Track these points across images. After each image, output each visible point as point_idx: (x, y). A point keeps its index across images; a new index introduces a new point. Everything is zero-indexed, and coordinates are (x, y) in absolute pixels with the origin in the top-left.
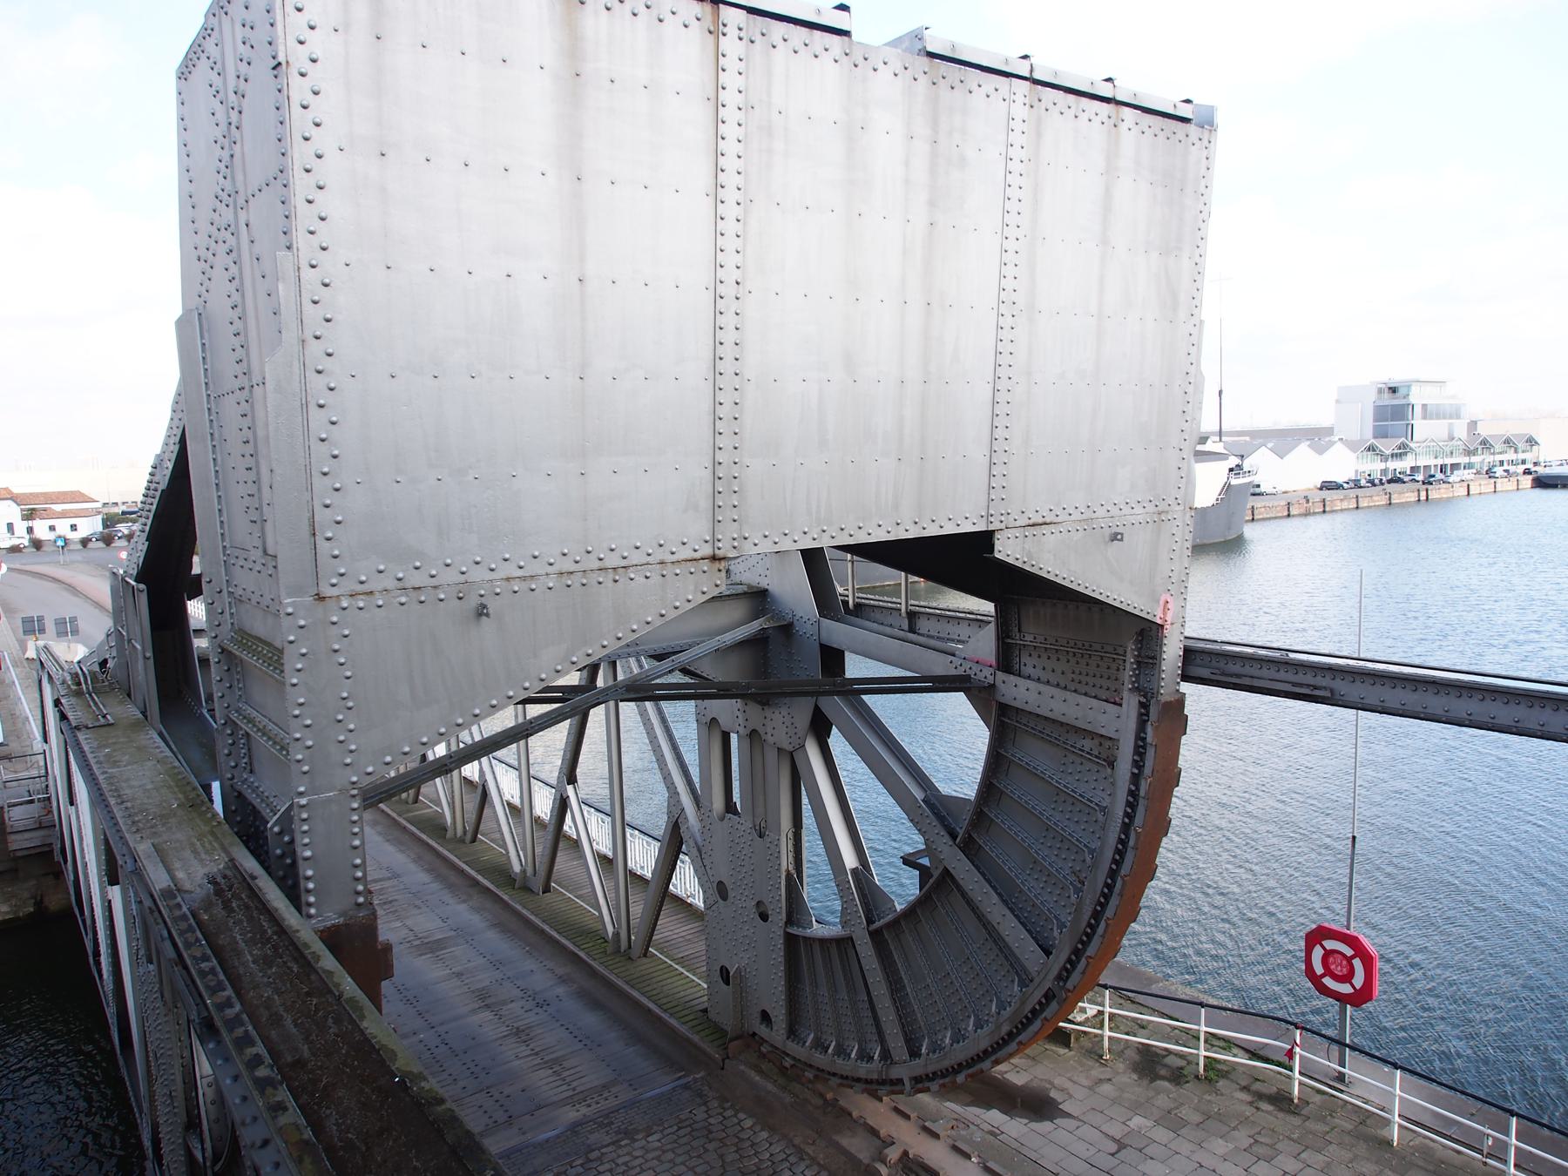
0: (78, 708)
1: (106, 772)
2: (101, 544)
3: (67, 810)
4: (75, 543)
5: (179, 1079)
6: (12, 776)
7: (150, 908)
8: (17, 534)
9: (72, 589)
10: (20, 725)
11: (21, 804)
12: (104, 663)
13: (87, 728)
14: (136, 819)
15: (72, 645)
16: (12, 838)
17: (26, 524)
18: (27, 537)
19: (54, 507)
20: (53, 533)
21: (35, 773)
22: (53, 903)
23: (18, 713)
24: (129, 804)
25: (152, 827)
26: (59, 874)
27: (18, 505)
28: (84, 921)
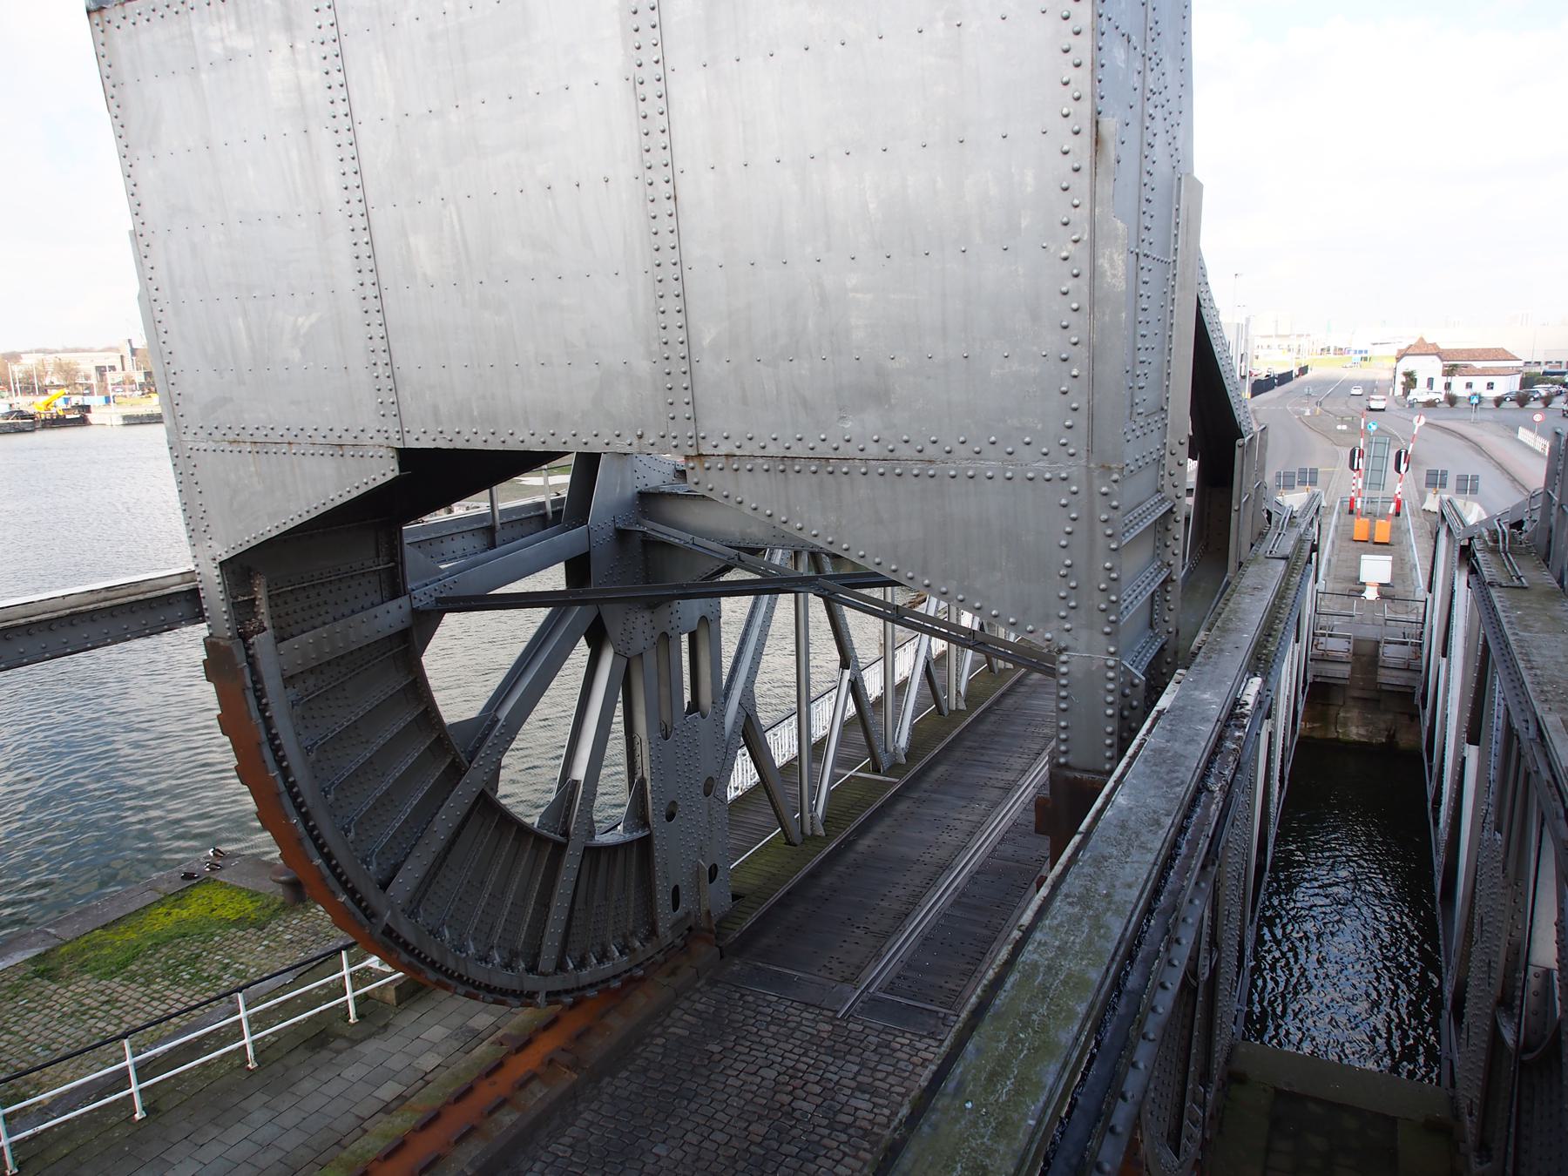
0: (1493, 565)
1: (1517, 634)
2: (1515, 405)
3: (1437, 661)
4: (1489, 401)
5: (1503, 955)
6: (1393, 616)
7: (1548, 782)
8: (1435, 389)
9: (1478, 448)
10: (1408, 571)
11: (1395, 643)
12: (1518, 525)
13: (1501, 586)
14: (1545, 688)
15: (1468, 503)
16: (1381, 671)
17: (1445, 380)
18: (1444, 392)
19: (1475, 364)
20: (1469, 390)
21: (1413, 618)
22: (1404, 740)
23: (1407, 559)
24: (1538, 672)
25: (1562, 701)
26: (1414, 717)
27: (1442, 360)
28: (1430, 768)
